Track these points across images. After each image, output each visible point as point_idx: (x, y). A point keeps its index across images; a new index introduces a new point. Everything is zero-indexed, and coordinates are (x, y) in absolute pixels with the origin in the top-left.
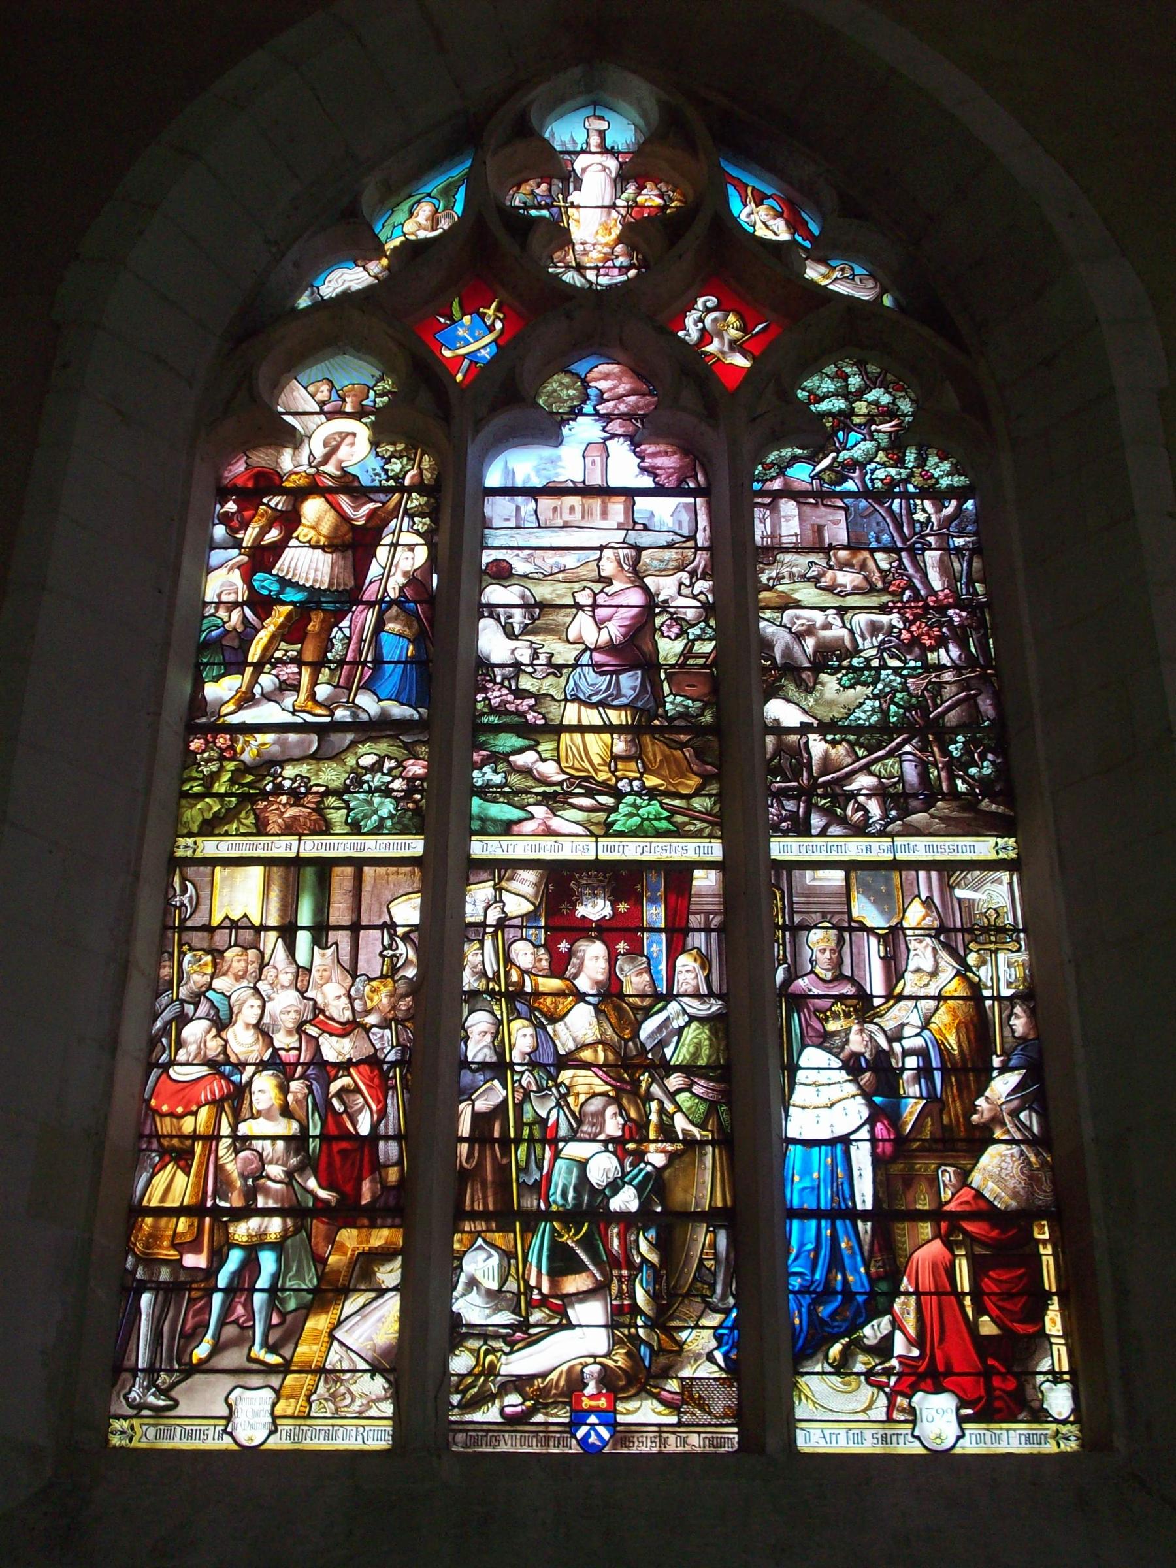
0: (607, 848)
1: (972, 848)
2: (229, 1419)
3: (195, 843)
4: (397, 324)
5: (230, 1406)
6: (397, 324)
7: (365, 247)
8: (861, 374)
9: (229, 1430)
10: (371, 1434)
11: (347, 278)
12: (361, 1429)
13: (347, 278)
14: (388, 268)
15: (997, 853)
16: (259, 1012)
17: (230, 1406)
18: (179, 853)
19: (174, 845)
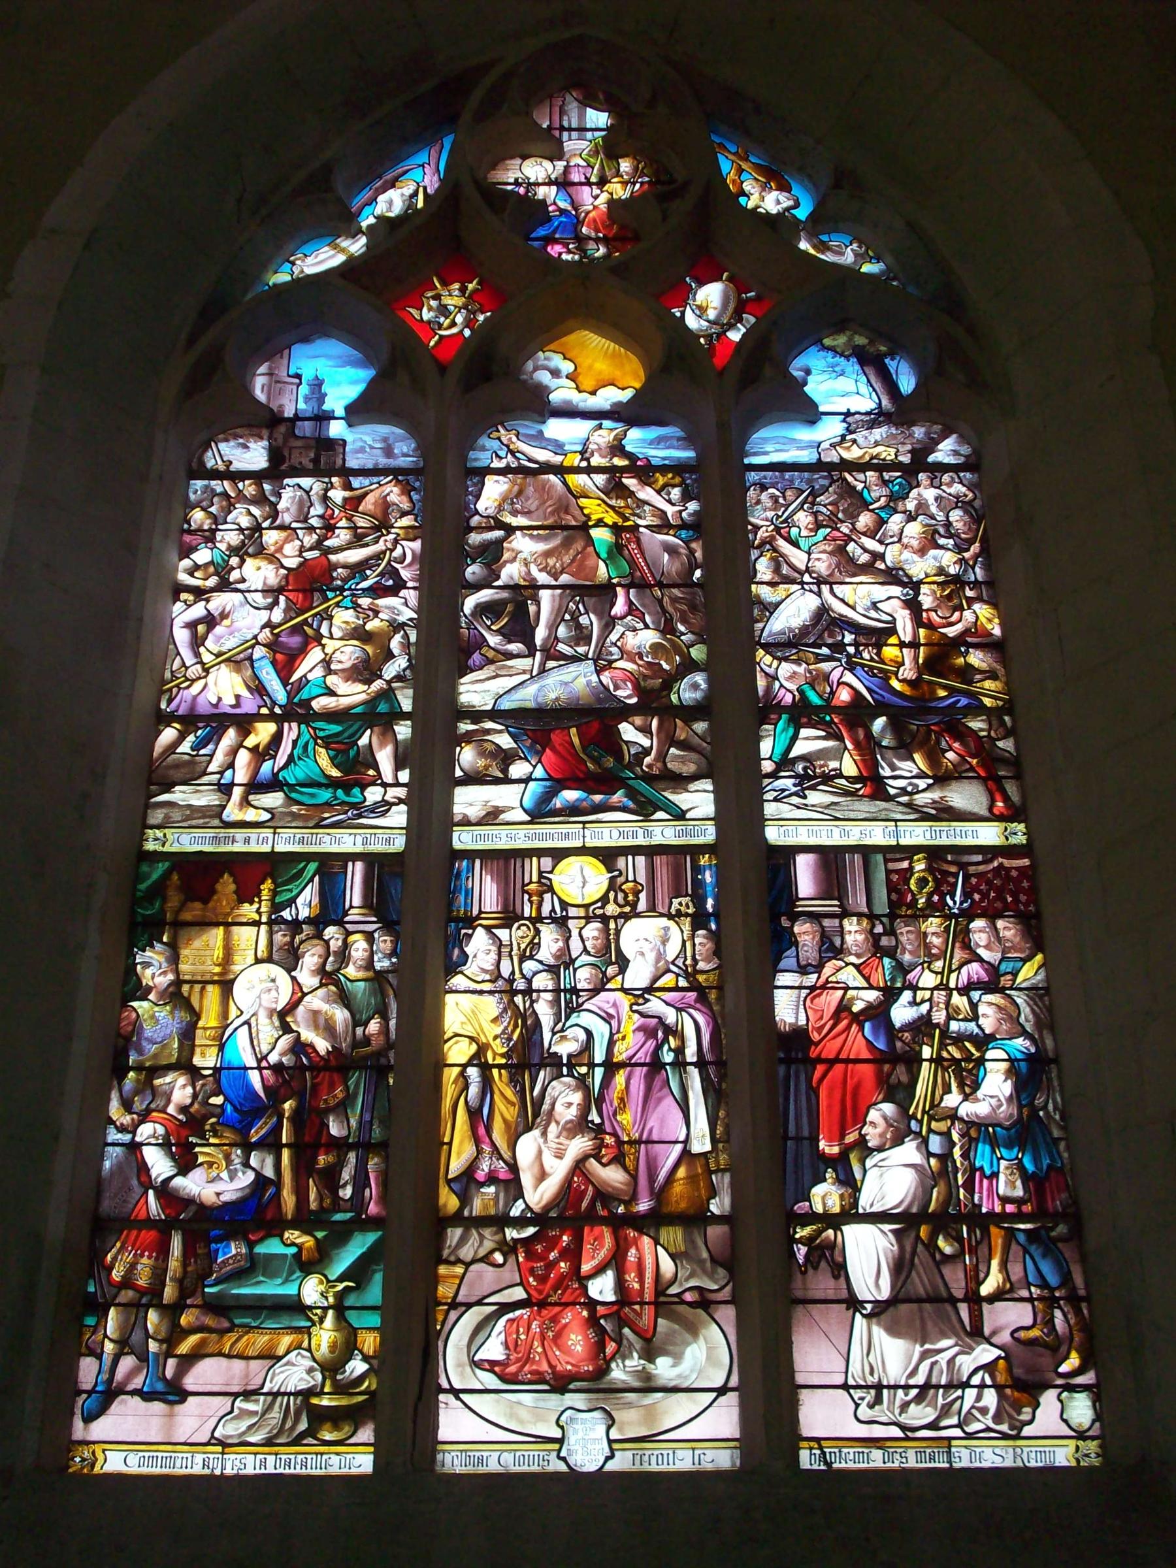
0: (594, 835)
1: (975, 835)
2: (561, 1441)
3: (165, 835)
4: (362, 305)
5: (562, 1428)
6: (362, 305)
7: (347, 224)
8: (856, 333)
9: (563, 1454)
10: (1033, 1455)
11: (321, 259)
12: (1018, 1450)
13: (321, 259)
14: (367, 245)
15: (1007, 839)
16: (496, 957)
17: (562, 1428)
18: (150, 846)
19: (142, 839)
